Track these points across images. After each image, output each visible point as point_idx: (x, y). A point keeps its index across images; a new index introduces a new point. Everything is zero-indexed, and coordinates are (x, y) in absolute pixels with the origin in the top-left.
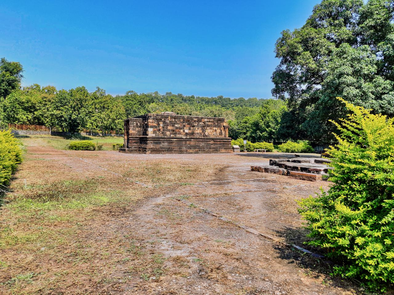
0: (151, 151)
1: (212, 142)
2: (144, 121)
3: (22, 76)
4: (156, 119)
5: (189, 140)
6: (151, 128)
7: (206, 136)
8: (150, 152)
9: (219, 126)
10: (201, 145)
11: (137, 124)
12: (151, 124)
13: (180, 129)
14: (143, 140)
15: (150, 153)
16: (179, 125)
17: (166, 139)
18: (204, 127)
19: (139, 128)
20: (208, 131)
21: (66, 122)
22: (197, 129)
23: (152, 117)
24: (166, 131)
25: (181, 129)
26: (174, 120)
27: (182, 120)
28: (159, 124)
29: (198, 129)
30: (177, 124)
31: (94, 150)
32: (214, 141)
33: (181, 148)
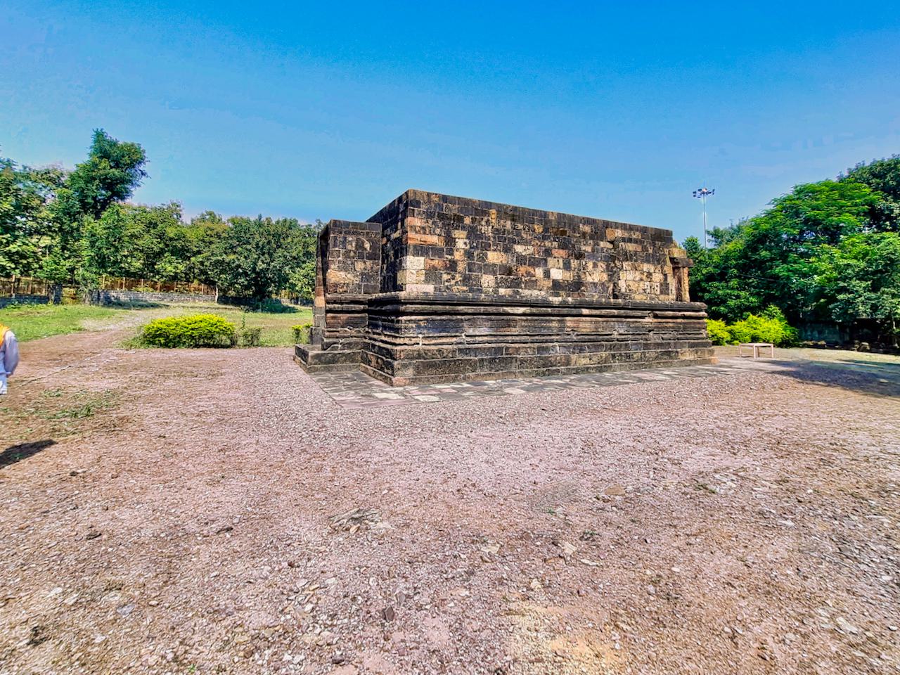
0: (418, 371)
1: (649, 321)
2: (388, 231)
3: (143, 174)
4: (442, 217)
5: (574, 311)
6: (416, 254)
7: (624, 296)
8: (410, 372)
9: (657, 260)
10: (615, 335)
11: (360, 246)
12: (418, 236)
13: (534, 263)
14: (383, 311)
15: (413, 381)
16: (531, 249)
17: (482, 309)
18: (613, 258)
19: (369, 263)
20: (628, 278)
21: (246, 276)
22: (590, 265)
23: (423, 208)
24: (480, 269)
25: (538, 266)
26: (509, 224)
27: (539, 228)
28: (450, 241)
29: (595, 265)
30: (526, 243)
31: (233, 344)
32: (656, 316)
33: (546, 349)
